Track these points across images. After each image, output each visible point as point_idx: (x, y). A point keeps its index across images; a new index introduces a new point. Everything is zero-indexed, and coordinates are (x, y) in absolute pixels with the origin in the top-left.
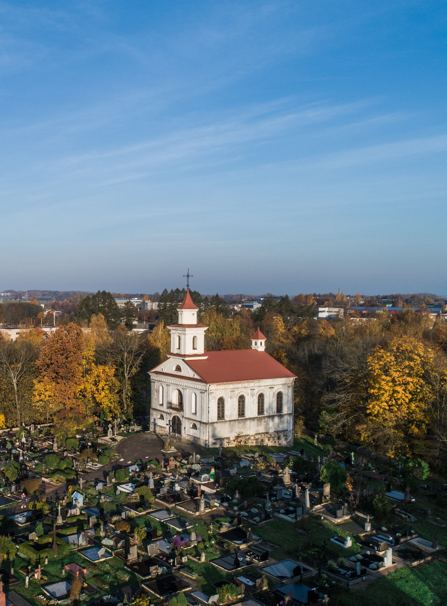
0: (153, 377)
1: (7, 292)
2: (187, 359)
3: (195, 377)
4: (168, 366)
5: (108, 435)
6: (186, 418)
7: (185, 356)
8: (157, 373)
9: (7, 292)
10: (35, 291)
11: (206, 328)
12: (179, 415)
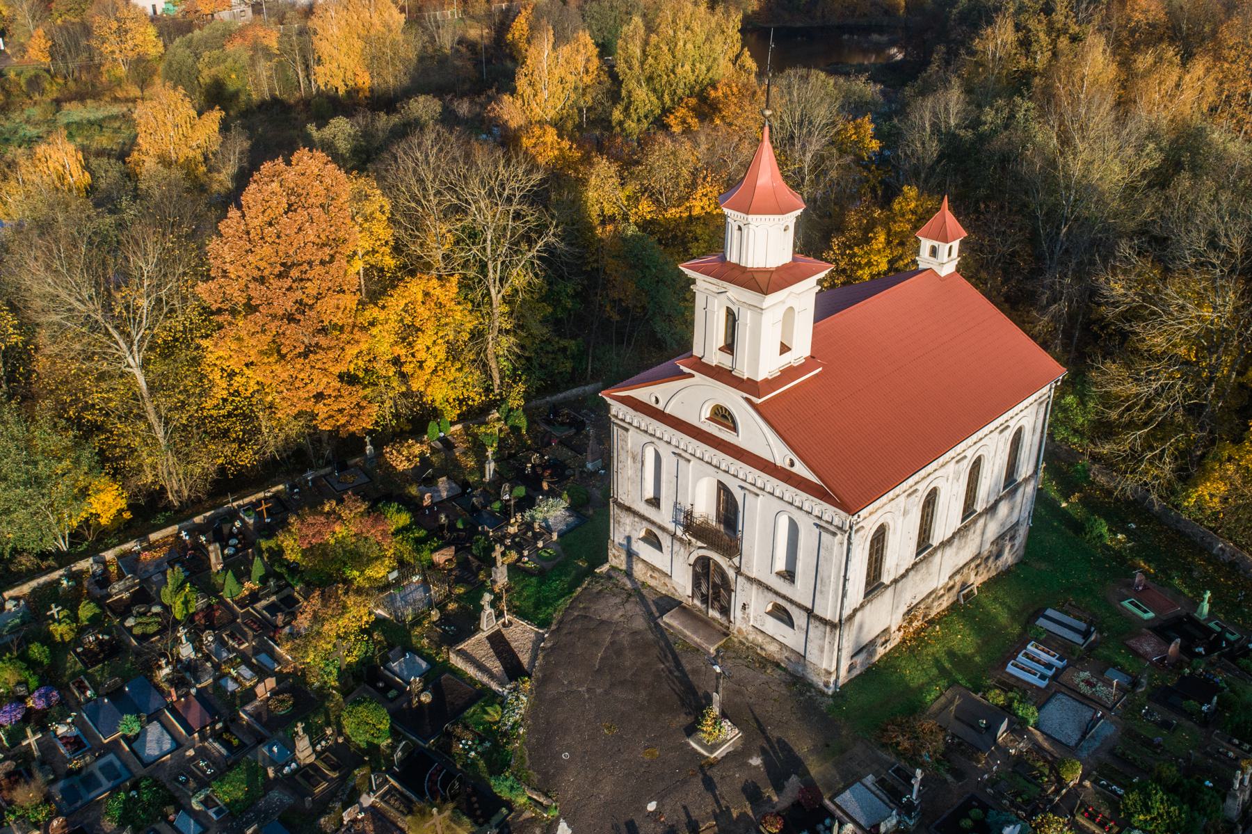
3: (794, 470)
4: (691, 398)
5: (484, 625)
6: (751, 580)
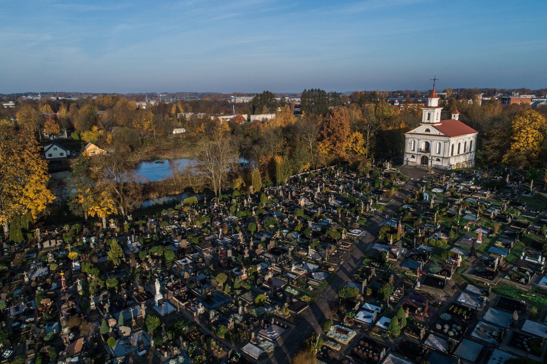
0: (407, 135)
1: (163, 94)
2: (435, 125)
4: (421, 129)
7: (433, 123)
8: (411, 134)
9: (163, 94)
10: (182, 93)
11: (442, 108)
12: (427, 155)
